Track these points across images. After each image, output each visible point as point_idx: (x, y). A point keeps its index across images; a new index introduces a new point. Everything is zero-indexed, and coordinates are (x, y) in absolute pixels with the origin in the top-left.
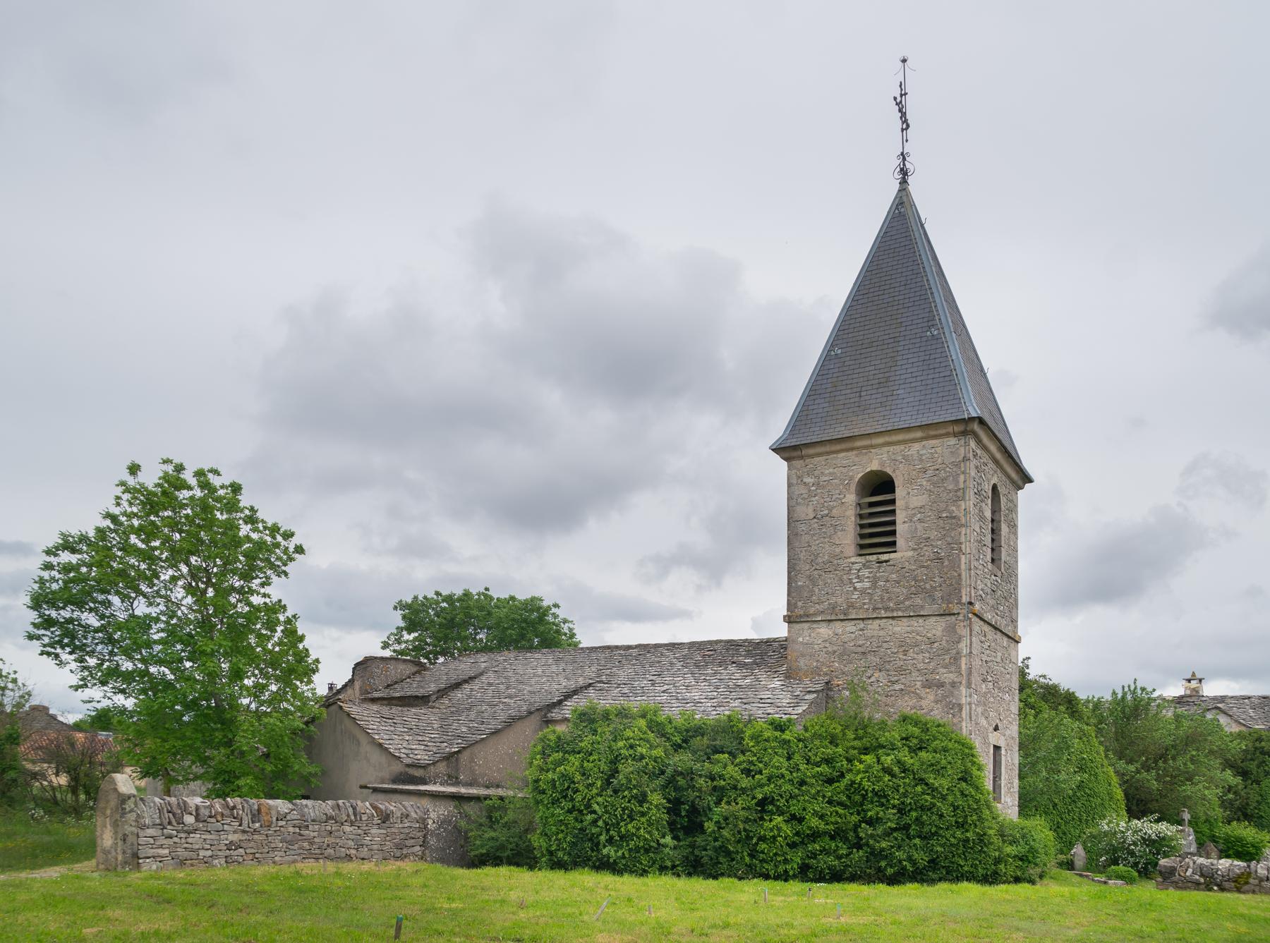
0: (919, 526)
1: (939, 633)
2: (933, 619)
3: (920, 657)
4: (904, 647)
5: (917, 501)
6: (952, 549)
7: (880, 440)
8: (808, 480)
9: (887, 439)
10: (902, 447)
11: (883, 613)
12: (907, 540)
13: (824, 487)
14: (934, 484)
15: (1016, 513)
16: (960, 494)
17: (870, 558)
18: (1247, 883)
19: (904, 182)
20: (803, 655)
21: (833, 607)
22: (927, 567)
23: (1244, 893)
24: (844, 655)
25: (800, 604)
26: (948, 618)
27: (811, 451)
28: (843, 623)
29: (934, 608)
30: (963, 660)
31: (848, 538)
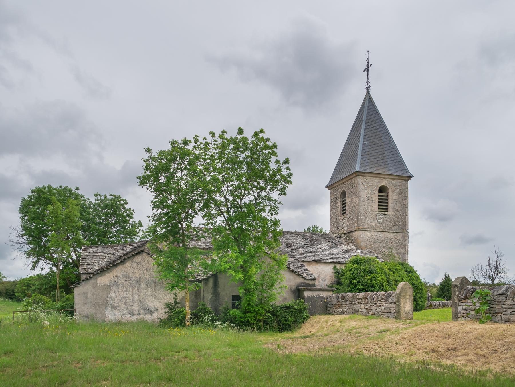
5: (395, 197)
9: (389, 177)
15: (407, 207)
19: (368, 91)
21: (372, 227)
27: (367, 175)
31: (376, 205)
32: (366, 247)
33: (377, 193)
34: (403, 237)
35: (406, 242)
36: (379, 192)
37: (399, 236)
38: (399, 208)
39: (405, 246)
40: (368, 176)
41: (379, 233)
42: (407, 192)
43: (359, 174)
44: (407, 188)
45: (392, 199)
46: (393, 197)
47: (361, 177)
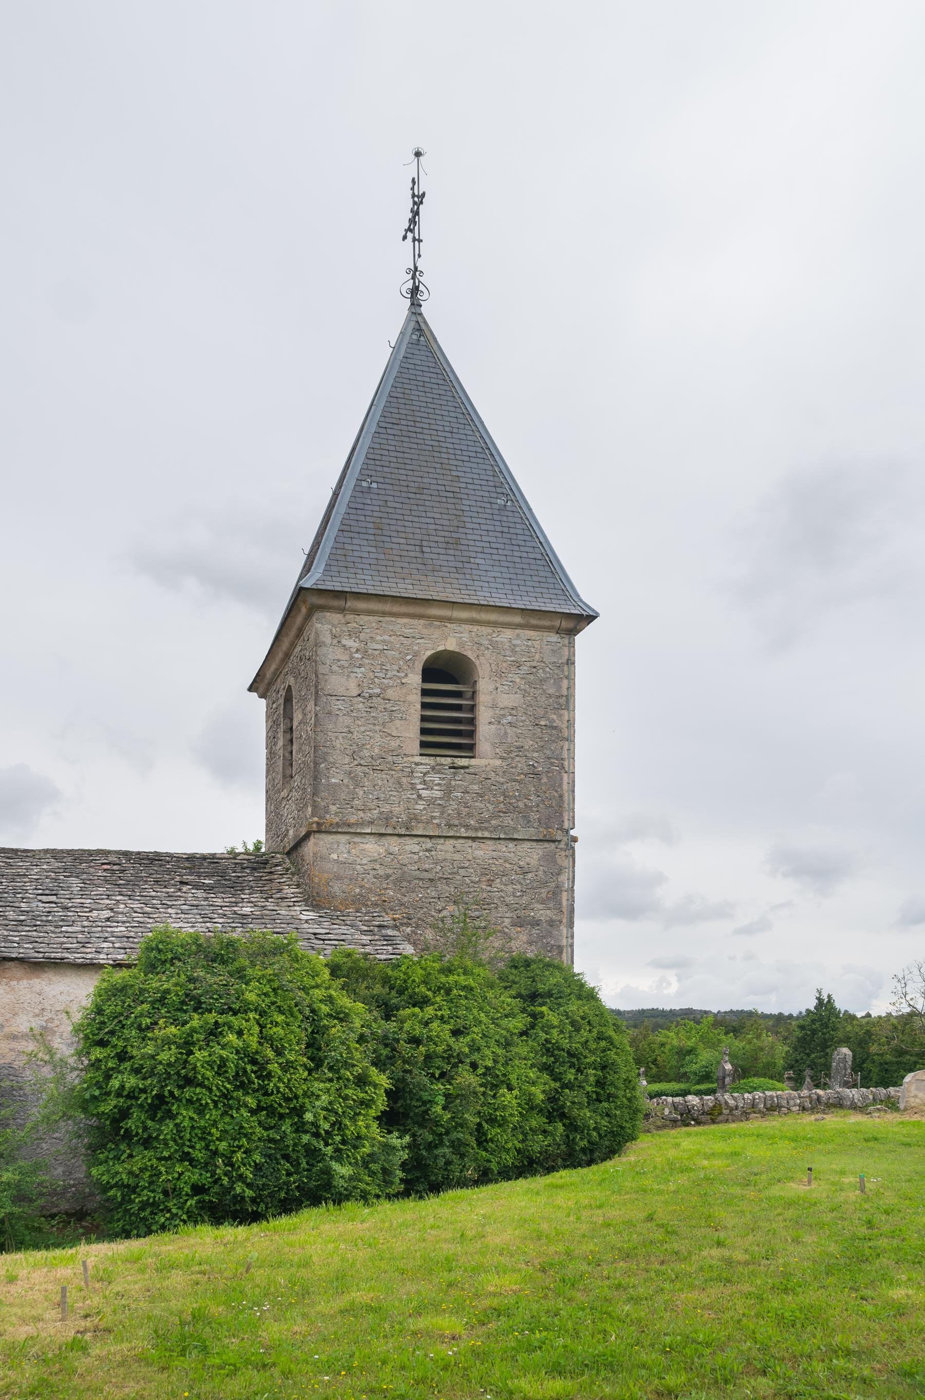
0: (510, 731)
1: (534, 862)
2: (527, 845)
3: (510, 888)
4: (488, 874)
5: (508, 700)
6: (552, 764)
7: (465, 614)
8: (349, 643)
9: (474, 615)
10: (489, 630)
11: (463, 832)
12: (494, 745)
13: (374, 658)
14: (530, 684)
15: (570, 739)
16: (562, 701)
17: (442, 760)
18: (720, 1114)
19: (415, 304)
20: (339, 878)
21: (387, 819)
22: (519, 782)
23: (718, 1123)
24: (401, 881)
25: (333, 808)
26: (546, 845)
27: (361, 605)
28: (402, 840)
29: (531, 832)
30: (565, 894)
31: (408, 730)
32: (359, 902)
33: (415, 679)
34: (550, 859)
35: (563, 878)
36: (425, 679)
37: (531, 855)
38: (528, 743)
39: (556, 893)
40: (370, 613)
41: (429, 844)
42: (570, 678)
43: (321, 601)
44: (570, 662)
45: (494, 706)
46: (495, 700)
47: (336, 617)
